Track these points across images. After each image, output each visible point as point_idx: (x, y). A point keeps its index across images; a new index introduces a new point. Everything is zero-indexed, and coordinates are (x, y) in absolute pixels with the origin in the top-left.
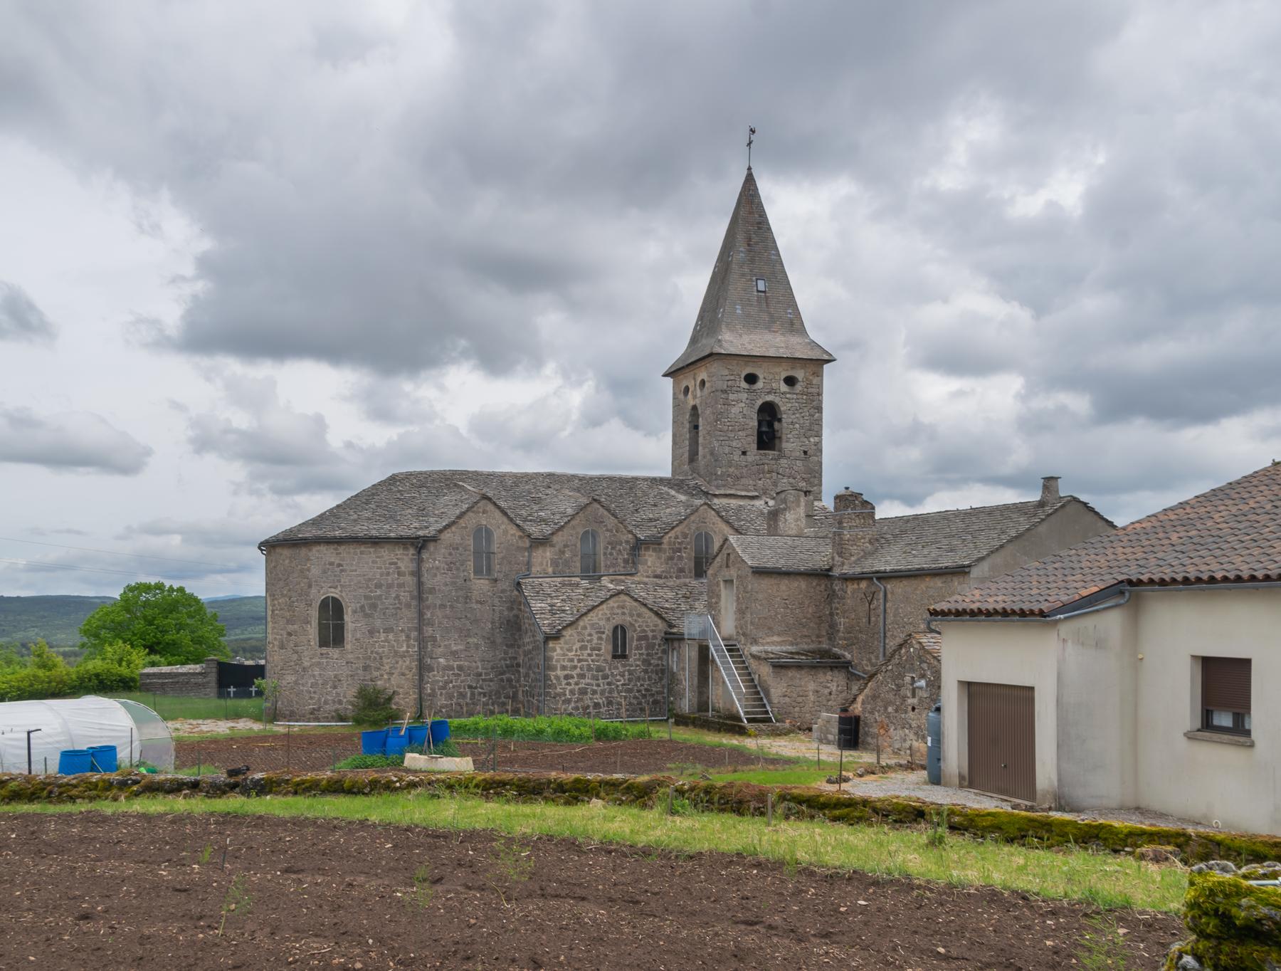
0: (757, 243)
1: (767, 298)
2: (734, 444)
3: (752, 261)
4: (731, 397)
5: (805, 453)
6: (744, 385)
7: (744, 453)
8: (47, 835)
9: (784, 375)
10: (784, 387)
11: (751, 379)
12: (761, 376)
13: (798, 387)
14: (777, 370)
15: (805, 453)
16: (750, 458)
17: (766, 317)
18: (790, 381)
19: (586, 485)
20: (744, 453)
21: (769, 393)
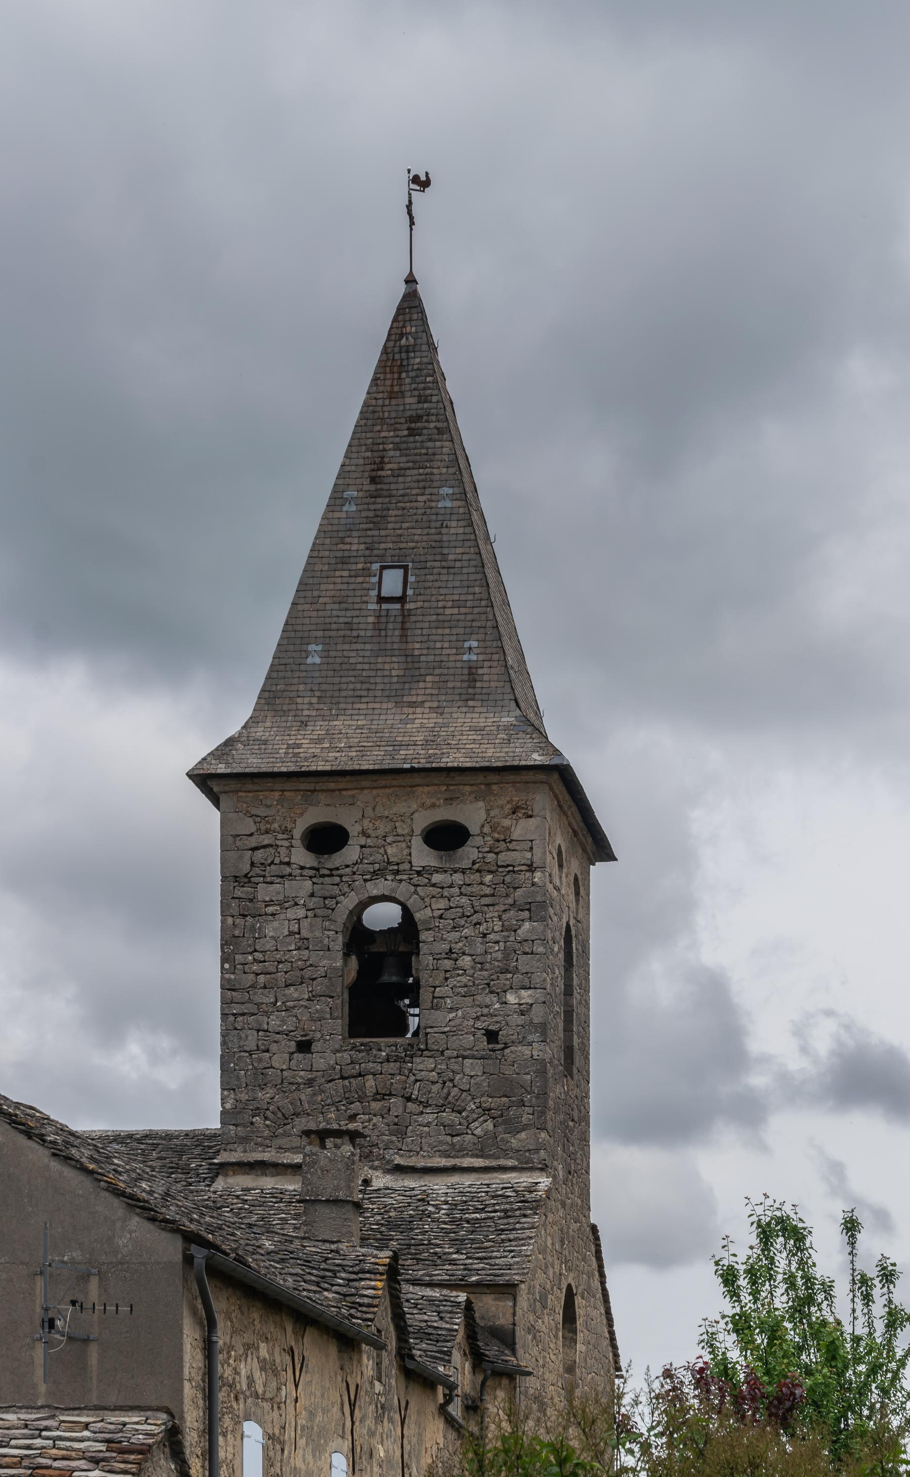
0: (400, 472)
1: (405, 615)
2: (274, 1022)
3: (378, 520)
4: (264, 892)
5: (492, 1036)
6: (301, 856)
7: (304, 1047)
8: (815, 1453)
9: (423, 820)
10: (423, 856)
11: (326, 839)
12: (353, 830)
13: (469, 853)
14: (400, 808)
15: (492, 1036)
16: (321, 1060)
17: (394, 668)
18: (446, 837)
19: (223, 1089)
20: (304, 1047)
21: (377, 874)
